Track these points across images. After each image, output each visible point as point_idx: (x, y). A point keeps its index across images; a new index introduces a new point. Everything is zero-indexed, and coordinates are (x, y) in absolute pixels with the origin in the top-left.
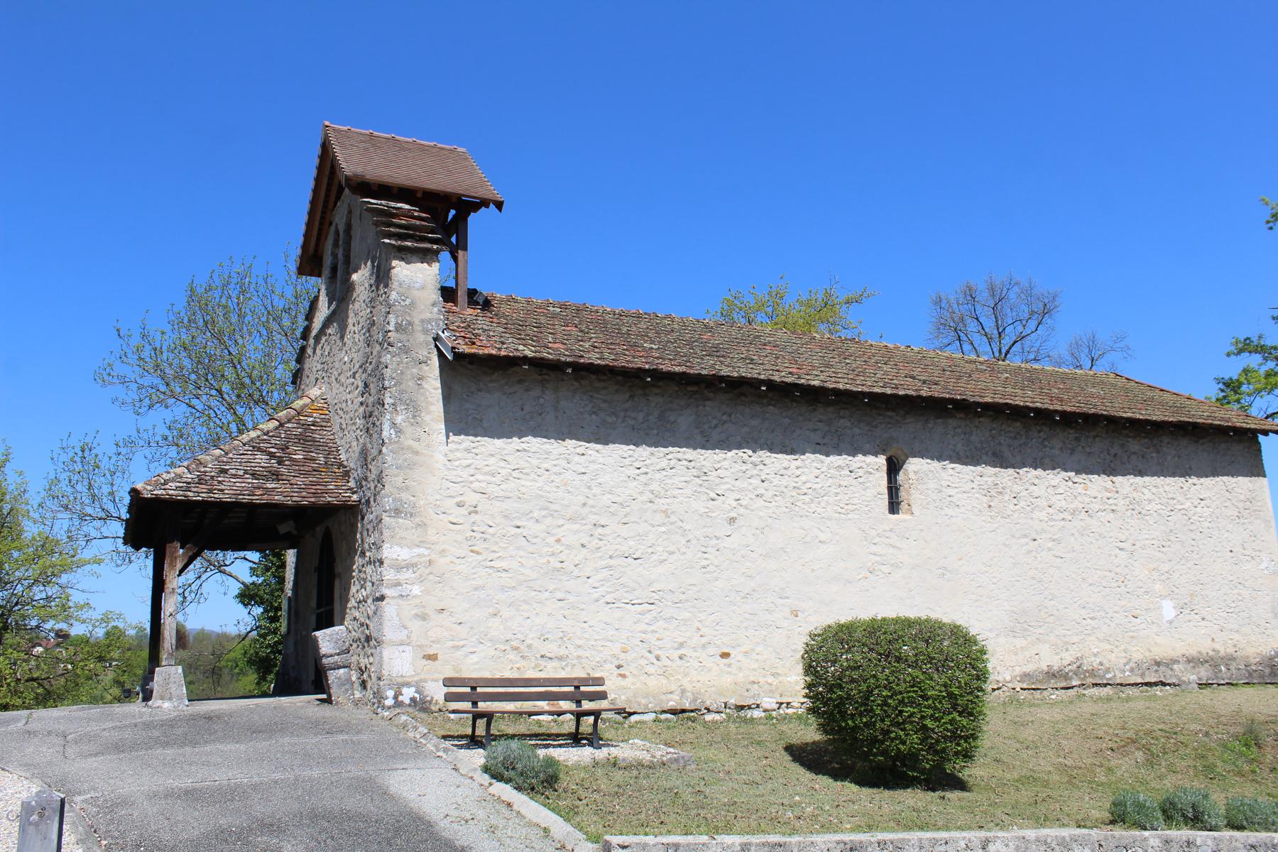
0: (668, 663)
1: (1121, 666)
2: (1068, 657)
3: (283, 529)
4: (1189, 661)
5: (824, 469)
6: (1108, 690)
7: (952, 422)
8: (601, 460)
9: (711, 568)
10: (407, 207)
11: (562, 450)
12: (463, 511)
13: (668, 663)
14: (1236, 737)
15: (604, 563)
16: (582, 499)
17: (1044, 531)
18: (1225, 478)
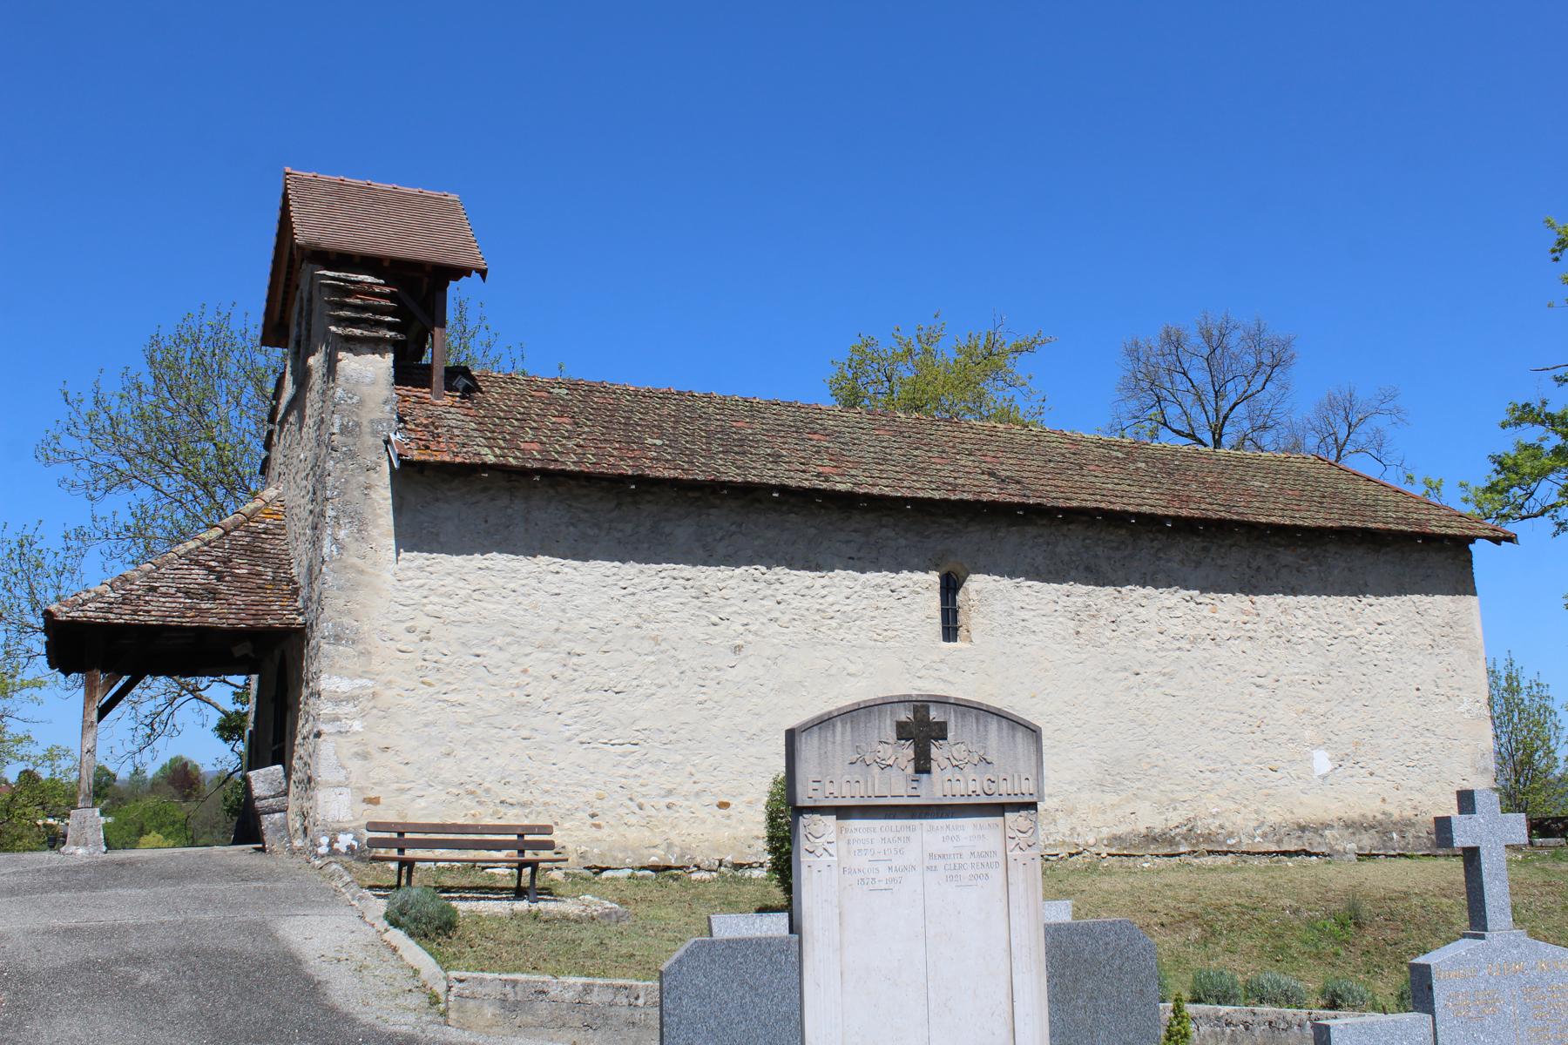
0: (654, 812)
1: (1250, 830)
2: (1175, 818)
3: (239, 651)
4: (1347, 826)
5: (858, 588)
6: (1229, 859)
7: (1031, 531)
8: (579, 579)
9: (709, 704)
10: (369, 279)
11: (532, 567)
12: (414, 637)
13: (654, 812)
14: (1331, 915)
15: (578, 697)
16: (555, 624)
17: (1150, 662)
18: (1416, 597)
